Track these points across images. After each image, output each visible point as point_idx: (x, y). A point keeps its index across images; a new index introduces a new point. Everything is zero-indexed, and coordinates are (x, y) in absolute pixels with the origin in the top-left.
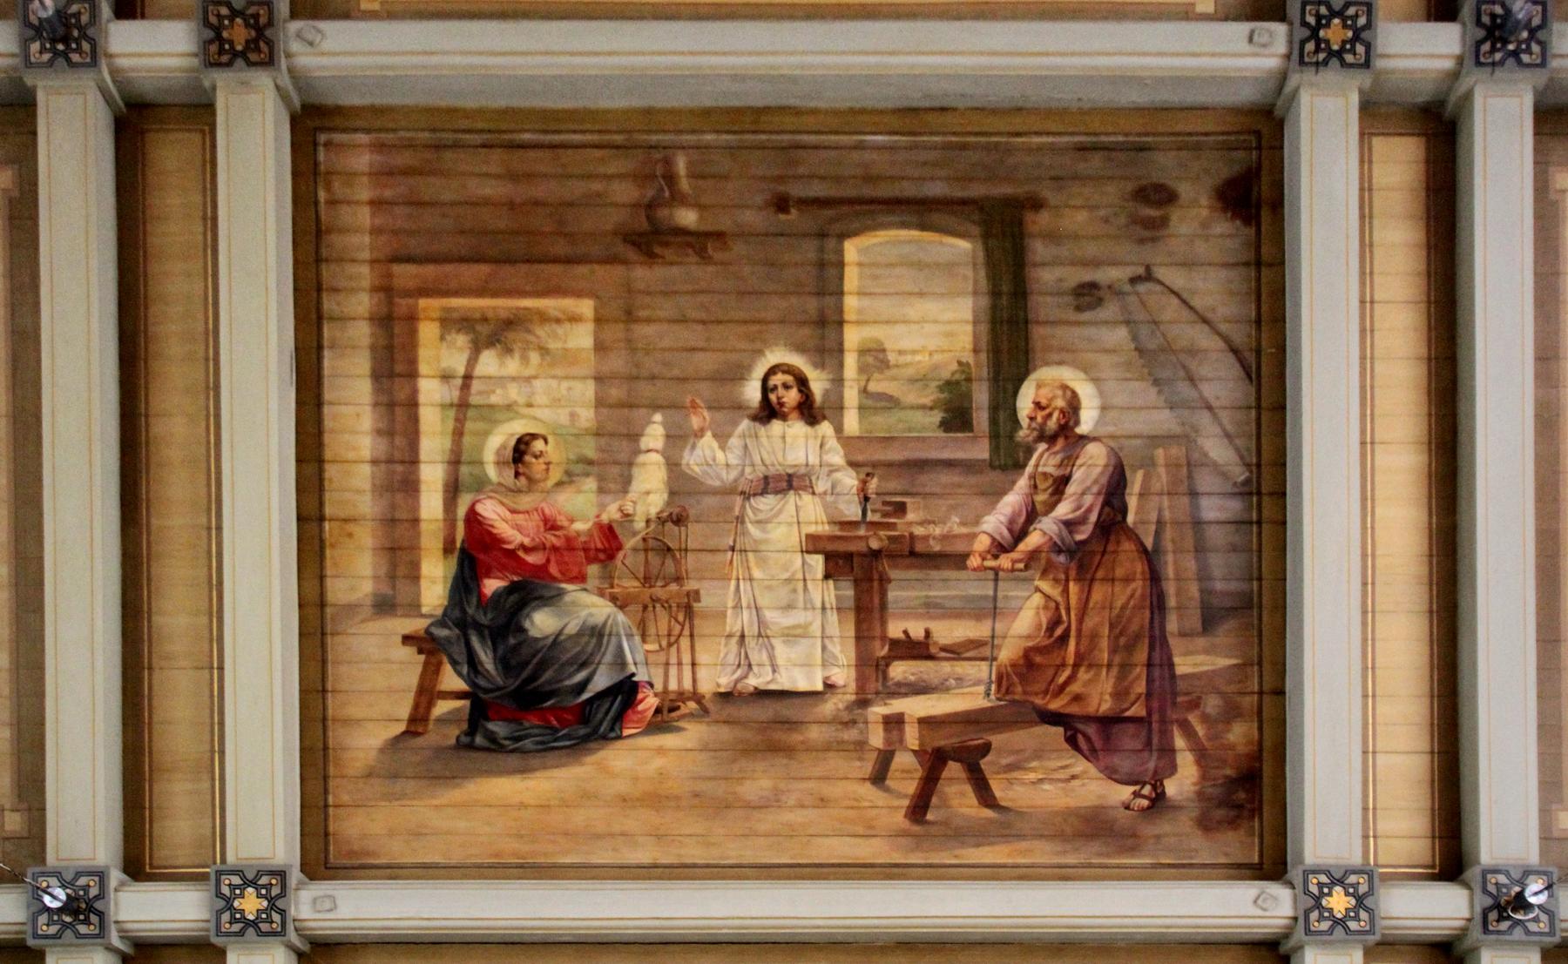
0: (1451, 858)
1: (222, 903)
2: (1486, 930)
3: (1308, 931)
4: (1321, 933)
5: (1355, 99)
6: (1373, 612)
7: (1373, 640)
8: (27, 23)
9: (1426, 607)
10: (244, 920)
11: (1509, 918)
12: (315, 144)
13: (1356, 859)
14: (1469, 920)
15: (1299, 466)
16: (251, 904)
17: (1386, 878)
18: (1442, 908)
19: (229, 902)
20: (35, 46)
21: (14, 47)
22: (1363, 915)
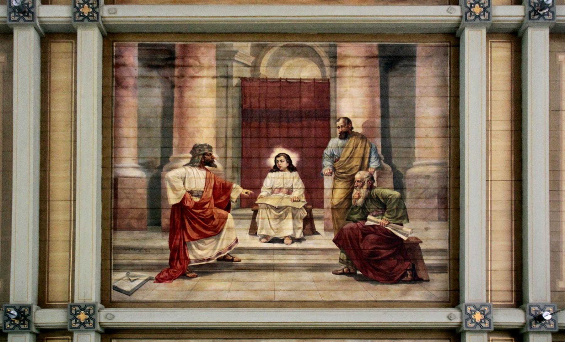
0: (519, 299)
1: (76, 10)
2: (530, 19)
3: (466, 20)
4: (471, 20)
5: (484, 31)
6: (491, 260)
7: (491, 71)
8: (10, 6)
10: (84, 16)
11: (539, 14)
12: (113, 46)
13: (484, 301)
14: (524, 16)
16: (82, 316)
17: (496, 306)
18: (514, 318)
19: (78, 9)
20: (13, 15)
21: (5, 14)
22: (486, 14)
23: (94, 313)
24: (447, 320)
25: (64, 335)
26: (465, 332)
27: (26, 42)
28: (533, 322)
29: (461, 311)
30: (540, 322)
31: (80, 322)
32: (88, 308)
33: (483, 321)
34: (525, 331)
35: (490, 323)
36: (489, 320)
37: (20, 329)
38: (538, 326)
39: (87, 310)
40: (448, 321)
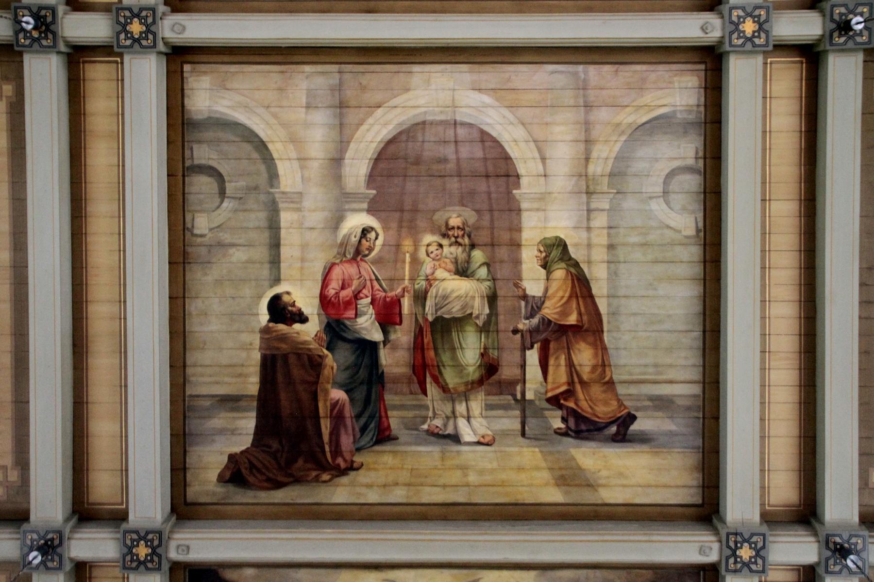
3: (731, 45)
9: (798, 282)
15: (725, 453)
23: (154, 22)
24: (700, 34)
25: (109, 55)
26: (728, 53)
27: (44, 74)
28: (836, 34)
29: (723, 17)
30: (846, 33)
31: (132, 37)
32: (144, 14)
33: (756, 34)
34: (821, 48)
35: (767, 37)
36: (767, 33)
37: (41, 46)
38: (842, 40)
39: (143, 18)
40: (702, 35)
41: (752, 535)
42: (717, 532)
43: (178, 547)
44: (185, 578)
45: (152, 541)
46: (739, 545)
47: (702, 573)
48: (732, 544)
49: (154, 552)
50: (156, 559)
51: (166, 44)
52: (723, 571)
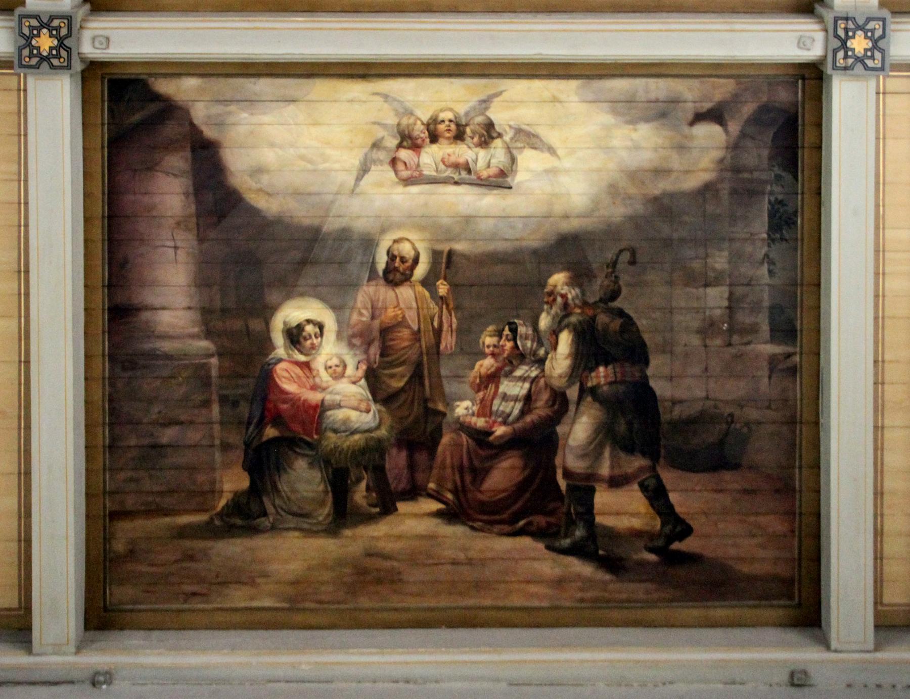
33: (869, 54)
41: (869, 20)
42: (821, 20)
43: (94, 39)
44: (103, 92)
45: (58, 29)
46: (850, 34)
47: (800, 82)
48: (841, 33)
49: (61, 45)
50: (64, 53)
51: (83, 60)
52: (829, 70)
